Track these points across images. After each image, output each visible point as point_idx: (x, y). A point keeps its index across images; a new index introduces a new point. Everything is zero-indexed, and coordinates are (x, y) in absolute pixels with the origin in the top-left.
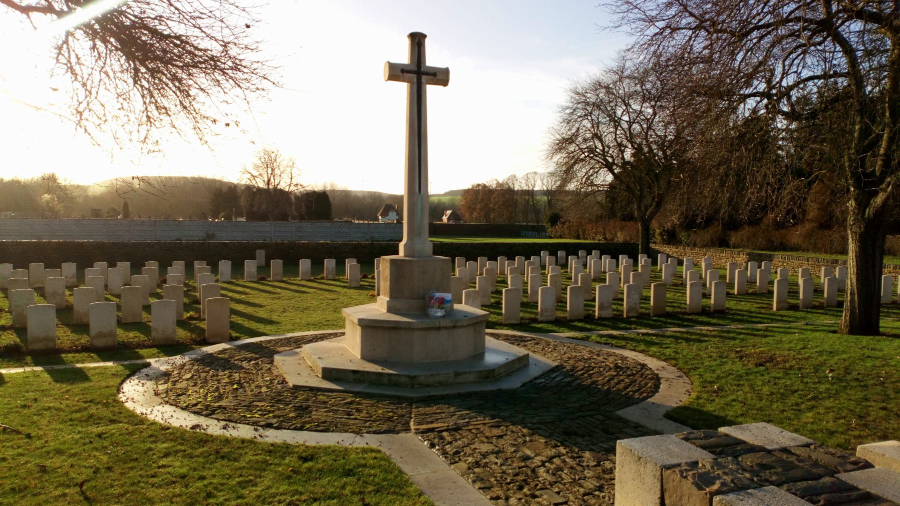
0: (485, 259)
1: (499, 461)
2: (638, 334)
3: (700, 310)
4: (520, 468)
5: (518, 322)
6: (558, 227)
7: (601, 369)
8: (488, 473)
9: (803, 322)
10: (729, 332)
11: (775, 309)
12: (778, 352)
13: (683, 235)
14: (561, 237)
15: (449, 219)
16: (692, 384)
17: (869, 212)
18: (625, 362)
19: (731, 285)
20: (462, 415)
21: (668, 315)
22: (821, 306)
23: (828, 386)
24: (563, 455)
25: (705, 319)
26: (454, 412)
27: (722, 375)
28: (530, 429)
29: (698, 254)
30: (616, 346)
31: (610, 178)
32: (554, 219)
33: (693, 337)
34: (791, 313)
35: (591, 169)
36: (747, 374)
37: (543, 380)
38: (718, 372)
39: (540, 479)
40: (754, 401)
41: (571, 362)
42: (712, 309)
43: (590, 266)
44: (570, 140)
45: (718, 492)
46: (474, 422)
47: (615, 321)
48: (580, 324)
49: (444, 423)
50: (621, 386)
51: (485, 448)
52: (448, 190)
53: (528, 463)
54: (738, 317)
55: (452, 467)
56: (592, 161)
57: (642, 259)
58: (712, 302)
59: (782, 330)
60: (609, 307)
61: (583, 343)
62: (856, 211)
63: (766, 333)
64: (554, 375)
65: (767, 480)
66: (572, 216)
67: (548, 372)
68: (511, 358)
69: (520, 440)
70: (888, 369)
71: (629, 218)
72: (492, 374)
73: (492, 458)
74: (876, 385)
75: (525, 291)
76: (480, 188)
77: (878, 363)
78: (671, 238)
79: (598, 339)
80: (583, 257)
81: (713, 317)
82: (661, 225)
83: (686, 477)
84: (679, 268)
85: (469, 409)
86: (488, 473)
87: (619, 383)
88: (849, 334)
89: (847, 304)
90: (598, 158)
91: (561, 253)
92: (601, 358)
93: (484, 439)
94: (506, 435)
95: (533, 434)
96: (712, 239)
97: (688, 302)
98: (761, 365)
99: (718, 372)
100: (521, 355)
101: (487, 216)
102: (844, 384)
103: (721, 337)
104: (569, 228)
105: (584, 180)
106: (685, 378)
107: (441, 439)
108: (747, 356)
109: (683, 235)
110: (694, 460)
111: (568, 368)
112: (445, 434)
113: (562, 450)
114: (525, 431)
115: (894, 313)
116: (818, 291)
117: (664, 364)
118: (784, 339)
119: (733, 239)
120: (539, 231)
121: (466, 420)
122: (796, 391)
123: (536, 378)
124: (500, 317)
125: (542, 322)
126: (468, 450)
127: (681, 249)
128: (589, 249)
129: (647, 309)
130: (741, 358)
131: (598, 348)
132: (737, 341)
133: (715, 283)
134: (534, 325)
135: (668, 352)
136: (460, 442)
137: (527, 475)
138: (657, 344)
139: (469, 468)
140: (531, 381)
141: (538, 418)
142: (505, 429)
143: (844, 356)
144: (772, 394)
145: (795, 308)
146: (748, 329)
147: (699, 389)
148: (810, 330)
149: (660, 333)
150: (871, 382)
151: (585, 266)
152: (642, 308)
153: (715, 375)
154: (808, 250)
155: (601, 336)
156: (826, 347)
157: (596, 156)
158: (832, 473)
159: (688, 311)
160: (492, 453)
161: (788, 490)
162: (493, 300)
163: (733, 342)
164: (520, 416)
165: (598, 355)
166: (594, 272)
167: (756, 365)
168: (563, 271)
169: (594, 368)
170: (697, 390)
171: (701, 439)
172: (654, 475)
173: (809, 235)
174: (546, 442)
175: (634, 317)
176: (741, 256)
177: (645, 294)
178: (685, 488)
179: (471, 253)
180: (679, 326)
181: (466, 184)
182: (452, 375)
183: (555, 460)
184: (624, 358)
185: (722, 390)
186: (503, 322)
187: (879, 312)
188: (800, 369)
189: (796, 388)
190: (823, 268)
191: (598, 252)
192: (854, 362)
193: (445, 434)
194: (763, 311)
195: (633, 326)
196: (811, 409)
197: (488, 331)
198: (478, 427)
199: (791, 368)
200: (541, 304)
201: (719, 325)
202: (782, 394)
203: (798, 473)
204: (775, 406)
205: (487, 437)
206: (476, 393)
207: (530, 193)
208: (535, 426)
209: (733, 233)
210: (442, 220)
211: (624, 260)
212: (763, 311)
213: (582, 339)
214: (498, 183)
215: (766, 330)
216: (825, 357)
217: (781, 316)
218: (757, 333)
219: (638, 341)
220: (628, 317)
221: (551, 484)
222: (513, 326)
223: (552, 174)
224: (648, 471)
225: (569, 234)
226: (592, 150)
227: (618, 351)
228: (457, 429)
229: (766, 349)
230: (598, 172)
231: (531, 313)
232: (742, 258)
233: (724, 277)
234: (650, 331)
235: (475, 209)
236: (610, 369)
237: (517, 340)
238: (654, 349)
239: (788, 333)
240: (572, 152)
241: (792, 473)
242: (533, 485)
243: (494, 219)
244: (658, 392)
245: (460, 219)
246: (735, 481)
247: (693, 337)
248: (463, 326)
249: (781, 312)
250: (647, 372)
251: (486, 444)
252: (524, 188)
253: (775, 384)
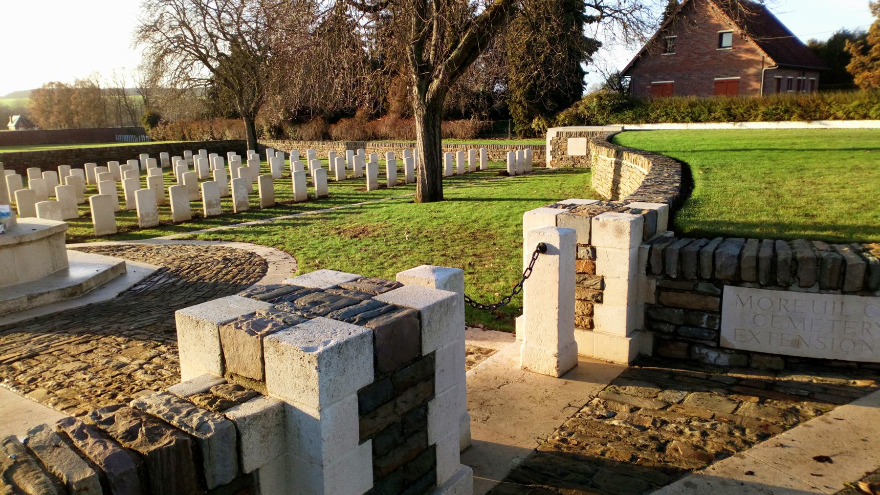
0: (67, 167)
1: (87, 377)
2: (248, 226)
3: (306, 198)
4: (113, 377)
5: (115, 232)
6: (160, 128)
7: (209, 265)
8: (74, 392)
9: (390, 197)
10: (330, 213)
11: (368, 189)
12: (369, 225)
13: (289, 130)
14: (164, 139)
15: (17, 126)
16: (297, 263)
17: (429, 96)
18: (234, 254)
19: (332, 173)
20: (39, 340)
21: (277, 205)
22: (403, 184)
23: (405, 245)
24: (164, 353)
25: (310, 205)
26: (30, 338)
27: (323, 250)
28: (125, 336)
29: (303, 147)
30: (226, 241)
31: (206, 73)
32: (154, 120)
33: (300, 222)
34: (380, 191)
35: (183, 61)
36: (344, 246)
37: (144, 286)
38: (320, 248)
39: (137, 382)
40: (349, 267)
41: (177, 263)
42: (316, 196)
43: (197, 166)
44: (154, 28)
45: (268, 333)
46: (55, 343)
47: (226, 217)
48: (187, 225)
49: (15, 353)
50: (228, 277)
51: (68, 368)
52: (11, 92)
53: (123, 370)
54: (339, 200)
55: (27, 396)
56: (184, 53)
57: (251, 154)
58: (316, 188)
59: (373, 206)
60: (217, 204)
61: (190, 242)
62: (419, 96)
63: (360, 210)
64: (156, 279)
65: (315, 314)
66: (168, 114)
67: (150, 277)
68: (102, 269)
69: (114, 350)
70: (447, 225)
71: (235, 115)
72: (79, 290)
73: (80, 375)
74: (439, 238)
75: (121, 199)
76: (54, 87)
77: (441, 221)
78: (279, 133)
79: (207, 237)
80: (189, 158)
81: (317, 203)
82: (268, 122)
83: (240, 328)
84: (286, 162)
85: (50, 332)
86: (74, 392)
87: (227, 274)
88: (424, 201)
89: (419, 178)
90: (188, 49)
91: (163, 156)
92: (209, 254)
93: (69, 359)
94: (96, 348)
95: (129, 341)
96: (316, 133)
97: (294, 192)
98: (355, 237)
99: (320, 248)
100: (115, 264)
101: (69, 119)
102: (417, 241)
103: (324, 218)
104: (171, 129)
105: (178, 73)
106: (291, 258)
107: (10, 371)
108: (344, 231)
109: (289, 130)
110: (253, 311)
111: (173, 269)
112: (16, 365)
113: (163, 348)
114: (120, 339)
115: (454, 183)
116: (400, 171)
117: (272, 249)
118: (374, 213)
119: (334, 132)
120: (137, 133)
121: (45, 344)
122: (381, 253)
123: (135, 286)
124: (92, 230)
125: (143, 228)
126: (48, 375)
127: (287, 143)
128: (195, 149)
129: (257, 202)
130: (339, 233)
131: (206, 245)
132: (337, 220)
134: (135, 233)
135: (275, 238)
136: (36, 369)
137: (121, 382)
138: (266, 232)
139: (49, 393)
140: (129, 289)
141: (136, 324)
142: (95, 342)
143: (418, 220)
144: (363, 258)
145: (383, 187)
146: (346, 208)
147: (303, 266)
148: (395, 203)
149: (270, 222)
150: (436, 237)
151: (191, 167)
152: (252, 202)
153: (317, 252)
154: (394, 138)
155: (210, 233)
156: (406, 215)
157: (188, 47)
158: (369, 296)
159: (295, 200)
160: (79, 370)
161: (331, 317)
162: (81, 213)
163: (333, 221)
164: (116, 326)
165: (206, 252)
166: (202, 171)
167: (351, 238)
168: (166, 174)
169: (201, 265)
170: (301, 267)
171: (264, 293)
172: (213, 335)
173: (394, 125)
174: (144, 345)
175: (244, 211)
176: (340, 146)
177: (254, 188)
178: (240, 338)
179: (48, 163)
180: (287, 214)
181: (38, 84)
182: (25, 300)
183: (154, 360)
184: (232, 251)
185: (322, 263)
186: (96, 234)
187: (442, 183)
188: (385, 235)
189: (381, 250)
190: (404, 151)
191: (205, 151)
192: (424, 223)
193: (16, 365)
194: (359, 192)
195: (244, 220)
196: (392, 265)
197: (68, 246)
198: (61, 347)
199: (378, 235)
200: (140, 209)
201: (323, 208)
202: (370, 258)
203: (342, 302)
204: (364, 269)
205: (73, 356)
206: (60, 314)
207: (122, 92)
208: (132, 333)
209: (333, 126)
210: (8, 128)
211: (232, 156)
212: (359, 192)
213: (190, 239)
214: (77, 81)
215: (361, 208)
216: (404, 223)
217: (373, 194)
218: (354, 211)
219: (248, 233)
220: (238, 212)
221: (149, 384)
222: (109, 237)
223: (140, 68)
224: (206, 332)
225: (173, 135)
226: (181, 39)
227: (227, 245)
228: (33, 355)
229: (359, 223)
230: (192, 64)
231: (130, 220)
232: (341, 148)
233: (327, 166)
234: (260, 222)
235: (51, 112)
236: (219, 262)
237: (113, 250)
238: (263, 237)
239: (377, 208)
240: (160, 42)
241: (337, 304)
242: (127, 389)
243: (79, 124)
244: (265, 275)
245: (32, 126)
246: (286, 320)
247: (300, 222)
248: (31, 242)
249: (373, 192)
250: (256, 259)
251: (71, 363)
252: (112, 87)
253: (366, 250)
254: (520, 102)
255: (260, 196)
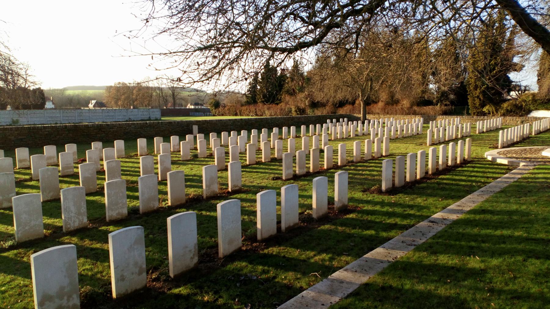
6: (221, 109)
15: (94, 106)
133: (214, 140)
181: (112, 82)
210: (88, 107)
254: (478, 97)
255: (181, 153)
